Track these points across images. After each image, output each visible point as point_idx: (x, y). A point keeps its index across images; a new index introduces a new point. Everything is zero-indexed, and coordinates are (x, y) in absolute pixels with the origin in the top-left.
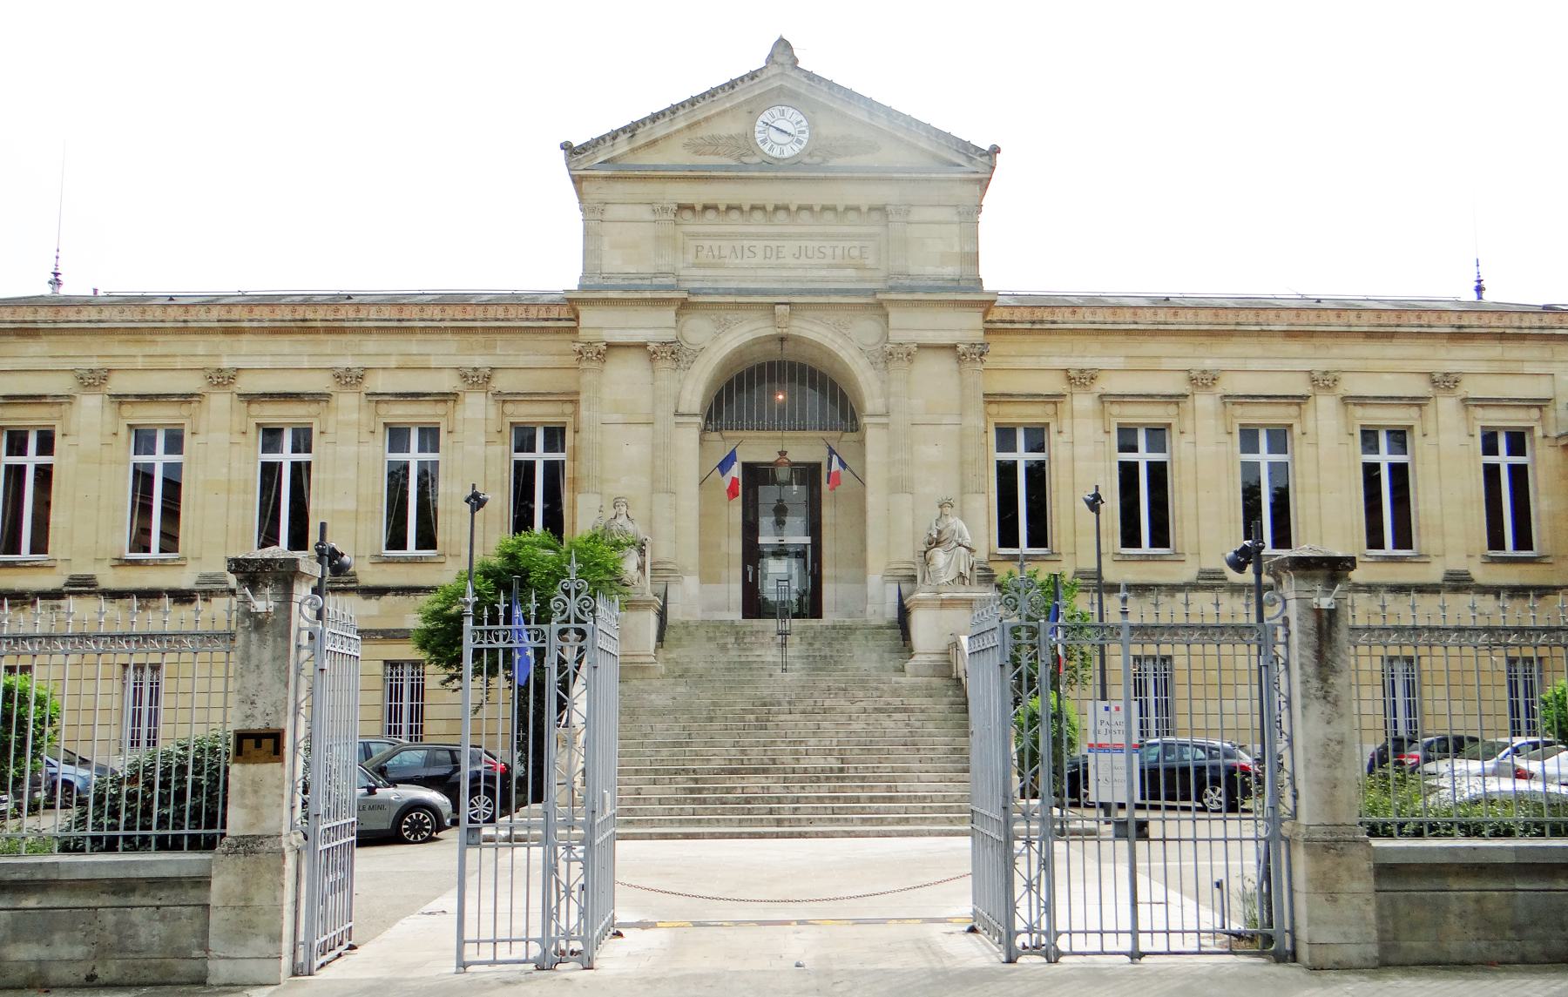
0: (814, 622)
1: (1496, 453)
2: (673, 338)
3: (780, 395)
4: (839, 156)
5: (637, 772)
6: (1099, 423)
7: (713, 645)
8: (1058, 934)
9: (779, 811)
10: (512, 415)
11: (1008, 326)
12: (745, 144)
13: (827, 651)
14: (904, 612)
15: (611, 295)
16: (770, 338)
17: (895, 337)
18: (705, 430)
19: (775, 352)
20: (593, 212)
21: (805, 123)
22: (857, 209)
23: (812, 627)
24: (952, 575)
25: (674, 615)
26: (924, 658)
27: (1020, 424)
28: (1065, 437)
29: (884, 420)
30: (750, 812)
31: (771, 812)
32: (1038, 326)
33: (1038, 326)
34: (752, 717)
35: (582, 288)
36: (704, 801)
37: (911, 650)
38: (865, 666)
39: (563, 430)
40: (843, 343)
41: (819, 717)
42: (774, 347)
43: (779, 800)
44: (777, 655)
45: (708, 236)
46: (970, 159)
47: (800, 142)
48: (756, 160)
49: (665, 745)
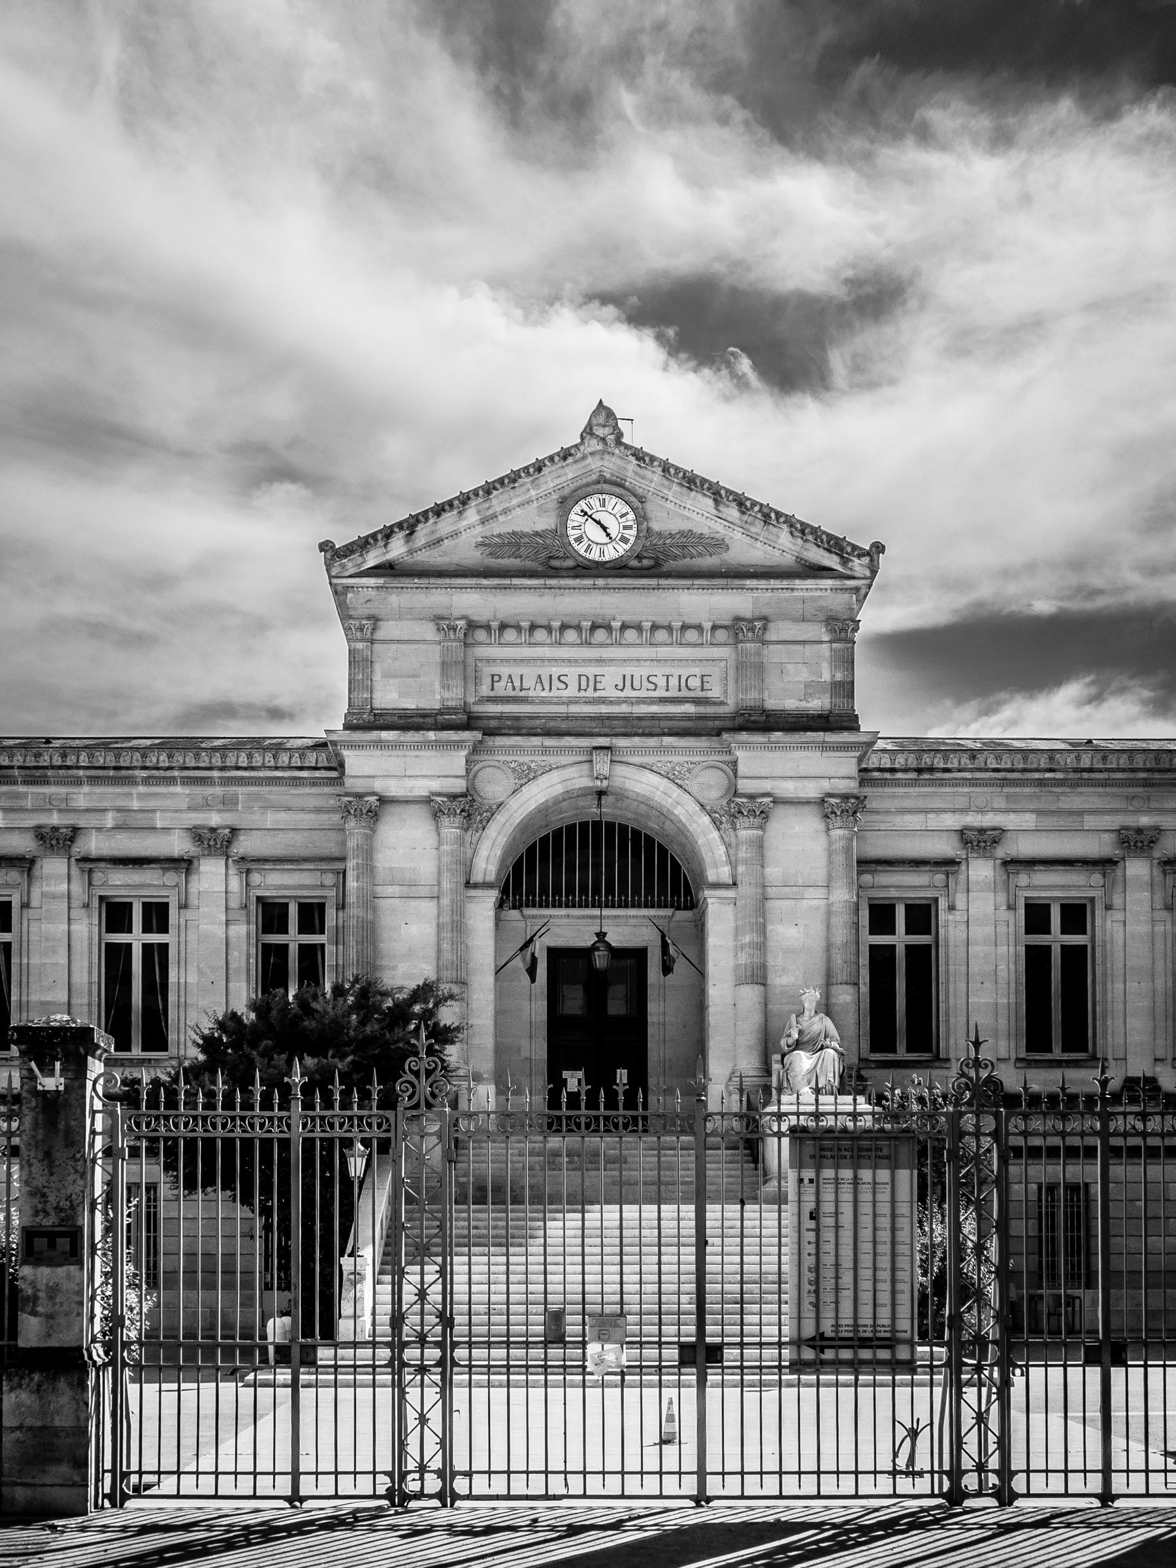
1: (1047, 931)
4: (675, 558)
8: (454, 1474)
11: (888, 775)
16: (584, 793)
18: (500, 905)
19: (591, 811)
21: (631, 516)
28: (958, 916)
39: (321, 907)
47: (624, 540)
48: (570, 563)
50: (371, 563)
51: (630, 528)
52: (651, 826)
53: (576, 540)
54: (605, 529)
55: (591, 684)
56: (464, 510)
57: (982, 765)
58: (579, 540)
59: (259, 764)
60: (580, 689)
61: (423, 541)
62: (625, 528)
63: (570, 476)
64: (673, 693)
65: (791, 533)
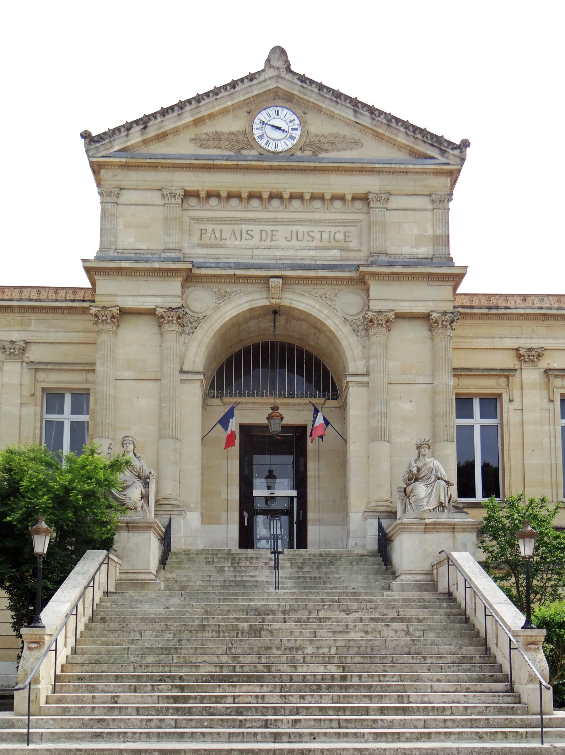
0: (302, 551)
2: (179, 305)
3: (276, 365)
4: (326, 151)
5: (117, 678)
6: (544, 393)
7: (210, 568)
9: (275, 724)
10: (43, 381)
11: (468, 311)
12: (245, 140)
13: (316, 573)
14: (384, 541)
15: (124, 264)
17: (375, 306)
20: (109, 195)
21: (297, 122)
22: (342, 198)
23: (301, 555)
24: (433, 504)
25: (177, 544)
26: (409, 577)
27: (476, 395)
28: (516, 405)
29: (364, 379)
30: (241, 724)
31: (266, 724)
32: (494, 311)
33: (494, 311)
34: (246, 625)
35: (98, 258)
36: (189, 711)
37: (394, 573)
38: (353, 585)
40: (330, 313)
41: (315, 626)
42: (266, 323)
43: (276, 711)
44: (270, 580)
45: (210, 220)
46: (443, 152)
47: (292, 138)
49: (151, 650)
50: (116, 148)
51: (296, 129)
52: (310, 343)
53: (259, 137)
54: (279, 128)
55: (269, 236)
56: (182, 113)
57: (531, 305)
58: (261, 137)
59: (45, 298)
60: (261, 240)
61: (153, 134)
62: (293, 129)
63: (255, 93)
64: (325, 243)
65: (406, 133)
